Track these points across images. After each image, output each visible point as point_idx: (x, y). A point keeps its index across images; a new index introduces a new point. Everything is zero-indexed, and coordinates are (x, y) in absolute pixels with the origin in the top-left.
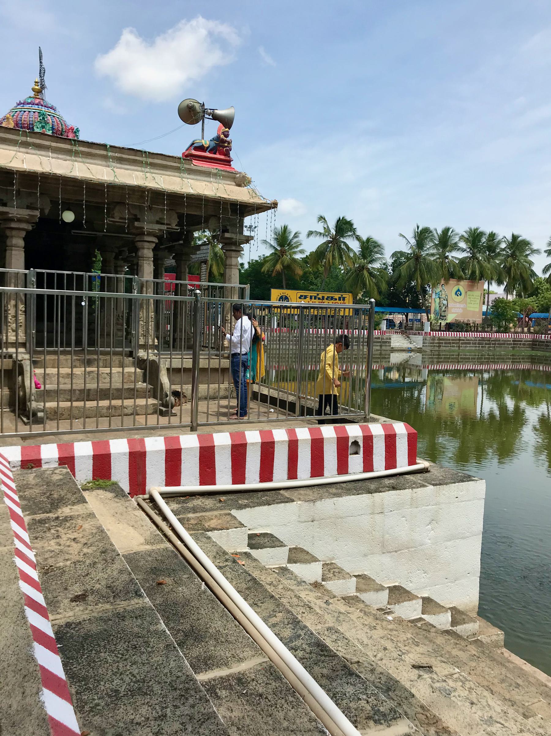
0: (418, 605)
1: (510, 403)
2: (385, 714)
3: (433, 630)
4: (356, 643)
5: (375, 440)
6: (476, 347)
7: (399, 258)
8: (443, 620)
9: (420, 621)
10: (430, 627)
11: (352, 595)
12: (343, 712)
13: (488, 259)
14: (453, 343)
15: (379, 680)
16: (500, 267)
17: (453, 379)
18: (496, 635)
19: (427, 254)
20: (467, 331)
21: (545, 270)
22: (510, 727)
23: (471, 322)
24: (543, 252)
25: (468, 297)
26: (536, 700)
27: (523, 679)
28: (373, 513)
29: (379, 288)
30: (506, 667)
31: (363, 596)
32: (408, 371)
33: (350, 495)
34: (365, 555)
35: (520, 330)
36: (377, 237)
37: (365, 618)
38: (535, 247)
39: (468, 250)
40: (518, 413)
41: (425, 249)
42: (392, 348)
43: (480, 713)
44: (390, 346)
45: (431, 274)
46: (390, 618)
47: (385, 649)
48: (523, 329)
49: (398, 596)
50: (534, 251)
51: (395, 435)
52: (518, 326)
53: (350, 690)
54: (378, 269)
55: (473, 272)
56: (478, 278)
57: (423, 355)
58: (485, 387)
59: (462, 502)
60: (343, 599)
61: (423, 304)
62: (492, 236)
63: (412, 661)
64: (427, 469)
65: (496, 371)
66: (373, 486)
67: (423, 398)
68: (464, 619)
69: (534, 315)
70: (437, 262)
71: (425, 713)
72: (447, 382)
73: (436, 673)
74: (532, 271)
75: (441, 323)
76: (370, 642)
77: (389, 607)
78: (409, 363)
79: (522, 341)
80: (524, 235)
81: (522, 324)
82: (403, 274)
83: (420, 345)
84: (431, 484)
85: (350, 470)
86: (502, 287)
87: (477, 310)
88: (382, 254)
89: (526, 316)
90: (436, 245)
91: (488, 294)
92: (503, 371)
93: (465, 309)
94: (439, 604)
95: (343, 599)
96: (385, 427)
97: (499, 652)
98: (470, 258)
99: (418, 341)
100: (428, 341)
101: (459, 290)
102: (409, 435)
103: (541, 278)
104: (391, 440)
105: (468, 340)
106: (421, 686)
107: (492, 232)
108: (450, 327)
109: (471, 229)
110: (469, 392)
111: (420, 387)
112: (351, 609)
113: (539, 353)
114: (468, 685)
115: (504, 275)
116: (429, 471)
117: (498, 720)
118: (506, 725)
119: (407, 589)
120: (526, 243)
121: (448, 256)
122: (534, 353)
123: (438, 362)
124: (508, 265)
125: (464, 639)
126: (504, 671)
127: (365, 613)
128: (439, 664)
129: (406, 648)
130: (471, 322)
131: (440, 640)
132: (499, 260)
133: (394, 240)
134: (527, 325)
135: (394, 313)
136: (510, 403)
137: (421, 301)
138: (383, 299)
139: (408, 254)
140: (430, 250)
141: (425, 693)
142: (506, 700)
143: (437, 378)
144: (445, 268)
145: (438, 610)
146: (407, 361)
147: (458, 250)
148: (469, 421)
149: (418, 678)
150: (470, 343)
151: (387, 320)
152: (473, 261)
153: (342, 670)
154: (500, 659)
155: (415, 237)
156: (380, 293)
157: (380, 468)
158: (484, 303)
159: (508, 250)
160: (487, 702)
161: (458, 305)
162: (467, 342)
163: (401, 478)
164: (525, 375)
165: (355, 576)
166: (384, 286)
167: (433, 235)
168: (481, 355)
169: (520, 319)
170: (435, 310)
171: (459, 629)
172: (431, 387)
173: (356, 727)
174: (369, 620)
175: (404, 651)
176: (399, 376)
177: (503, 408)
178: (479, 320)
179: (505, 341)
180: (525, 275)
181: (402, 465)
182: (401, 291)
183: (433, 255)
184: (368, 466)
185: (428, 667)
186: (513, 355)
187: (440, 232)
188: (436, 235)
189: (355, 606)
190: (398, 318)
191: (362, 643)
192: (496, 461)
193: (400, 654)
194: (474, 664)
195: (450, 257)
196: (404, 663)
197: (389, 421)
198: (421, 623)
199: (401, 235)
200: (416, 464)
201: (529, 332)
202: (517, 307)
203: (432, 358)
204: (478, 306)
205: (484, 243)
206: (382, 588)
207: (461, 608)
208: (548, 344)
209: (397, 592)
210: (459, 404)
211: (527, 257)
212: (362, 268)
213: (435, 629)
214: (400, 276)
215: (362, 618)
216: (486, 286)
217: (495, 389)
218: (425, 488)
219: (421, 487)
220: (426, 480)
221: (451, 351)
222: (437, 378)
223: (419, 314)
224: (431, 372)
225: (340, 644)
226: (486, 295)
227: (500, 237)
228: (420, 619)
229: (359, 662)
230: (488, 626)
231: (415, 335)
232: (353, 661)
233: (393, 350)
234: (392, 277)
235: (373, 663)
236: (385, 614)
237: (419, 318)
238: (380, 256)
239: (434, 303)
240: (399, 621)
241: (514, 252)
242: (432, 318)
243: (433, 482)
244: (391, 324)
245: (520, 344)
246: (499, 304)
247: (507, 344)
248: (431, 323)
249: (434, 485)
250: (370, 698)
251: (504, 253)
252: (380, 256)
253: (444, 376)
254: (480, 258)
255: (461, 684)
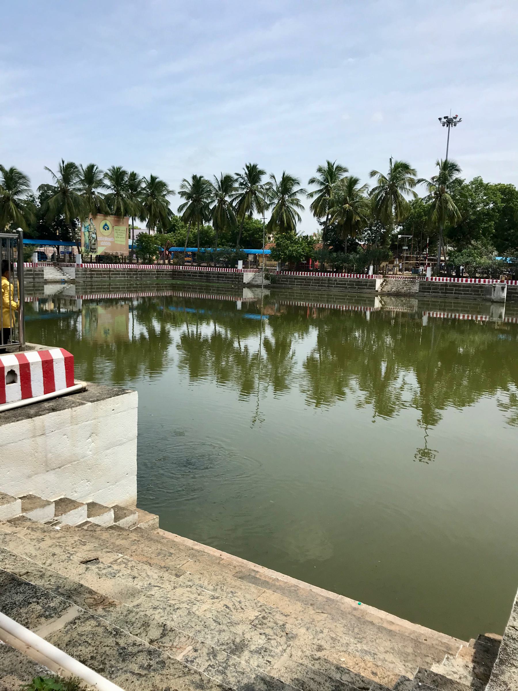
0: (83, 511)
1: (157, 326)
2: (55, 608)
3: (99, 528)
4: (24, 556)
5: (32, 368)
6: (125, 277)
7: (46, 191)
8: (106, 519)
9: (86, 524)
10: (95, 527)
11: (18, 516)
12: (14, 619)
13: (131, 197)
14: (104, 274)
15: (49, 583)
16: (142, 205)
17: (106, 307)
18: (153, 519)
19: (74, 189)
20: (116, 263)
21: (180, 209)
22: (166, 587)
23: (119, 254)
24: (177, 193)
25: (115, 231)
26: (185, 562)
27: (175, 548)
28: (34, 436)
29: (27, 220)
30: (161, 543)
31: (29, 515)
32: (62, 302)
33: (9, 423)
34: (29, 477)
35: (161, 262)
36: (21, 168)
37: (32, 533)
38: (170, 188)
39: (113, 187)
40: (164, 334)
41: (72, 183)
42: (46, 280)
43: (141, 584)
44: (43, 278)
45: (79, 209)
46: (58, 528)
47: (54, 555)
48: (164, 262)
49: (64, 507)
50: (169, 192)
51: (52, 361)
52: (160, 258)
53: (20, 598)
54: (25, 201)
55: (119, 209)
56: (123, 213)
57: (76, 286)
58: (135, 313)
59: (118, 413)
60: (8, 521)
61: (74, 237)
62: (133, 176)
63: (80, 559)
64: (85, 388)
65: (143, 298)
66: (32, 411)
67: (79, 327)
68: (125, 514)
69: (172, 249)
70: (84, 197)
71: (93, 596)
72: (101, 310)
73: (102, 563)
74: (169, 209)
75: (91, 256)
76: (38, 553)
77: (56, 518)
78: (64, 294)
79: (164, 272)
80: (161, 177)
81: (163, 256)
82: (51, 207)
83: (73, 277)
84: (89, 401)
85: (8, 399)
86: (145, 223)
87: (124, 243)
88: (27, 186)
89: (166, 250)
90: (81, 180)
91: (133, 229)
92: (150, 298)
93: (113, 243)
94: (102, 506)
95: (8, 521)
96: (41, 353)
97: (156, 533)
98: (115, 195)
99: (71, 273)
100: (80, 273)
101: (106, 225)
102: (66, 359)
103: (177, 216)
104: (48, 366)
105: (118, 271)
106: (89, 576)
107: (133, 172)
108: (100, 259)
109: (114, 168)
110: (120, 319)
111: (75, 317)
112: (17, 529)
113: (179, 282)
114: (130, 565)
115: (145, 212)
116: (87, 390)
117: (156, 585)
118: (162, 586)
119: (73, 499)
120: (162, 185)
121: (94, 192)
122: (174, 282)
123: (91, 293)
124: (148, 203)
125: (126, 530)
126: (159, 546)
127: (33, 529)
128: (105, 555)
129: (74, 550)
130: (119, 254)
131: (105, 535)
132: (140, 198)
133: (40, 174)
134: (168, 258)
135: (45, 245)
136: (157, 326)
137: (71, 234)
138: (33, 231)
139: (55, 187)
140: (76, 185)
141: (92, 581)
142: (161, 567)
143: (91, 307)
144: (92, 203)
145: (102, 511)
146: (62, 292)
147: (103, 187)
148: (123, 344)
149: (86, 571)
150: (119, 274)
151: (38, 252)
152: (118, 198)
153: (10, 583)
154: (156, 538)
155: (61, 171)
156: (29, 225)
157: (38, 393)
158: (129, 238)
159: (148, 190)
160: (146, 573)
161: (106, 239)
162: (117, 273)
163: (60, 400)
164: (168, 301)
165: (20, 498)
166: (32, 219)
167: (78, 171)
168: (130, 285)
169: (161, 253)
170: (85, 243)
171: (121, 523)
172: (86, 316)
173: (28, 628)
174: (38, 534)
175: (72, 553)
176: (55, 307)
177: (151, 331)
178: (126, 252)
179: (150, 271)
180: (163, 213)
181: (61, 387)
182: (50, 225)
183: (80, 190)
184: (26, 392)
185: (95, 559)
186: (157, 284)
187: (85, 167)
188: (81, 171)
189: (21, 525)
190: (50, 251)
191: (30, 556)
192: (147, 377)
193: (69, 556)
194: (134, 547)
195: (96, 193)
196: (73, 562)
197: (45, 348)
198: (87, 526)
199: (47, 168)
200: (74, 385)
201: (169, 263)
202: (158, 241)
203: (86, 288)
204: (124, 240)
205: (126, 182)
206: (48, 503)
207: (122, 505)
208: (185, 274)
209: (63, 504)
210: (113, 330)
211: (164, 197)
212: (7, 199)
213: (100, 528)
214: (48, 209)
215: (30, 534)
216: (130, 222)
217: (144, 313)
218: (84, 406)
219: (80, 405)
220: (84, 399)
221: (101, 282)
222: (91, 307)
223: (70, 247)
224: (85, 302)
225: (7, 562)
226: (131, 230)
227: (140, 177)
228: (87, 522)
229: (28, 572)
230: (146, 514)
231: (67, 266)
232: (21, 573)
233: (47, 282)
234: (40, 209)
235: (42, 570)
236: (52, 526)
237: (70, 250)
238: (26, 188)
239: (84, 237)
240: (67, 528)
241: (153, 192)
242: (83, 251)
243: (91, 400)
244: (42, 256)
245: (163, 274)
246: (142, 237)
247: (152, 274)
248: (82, 255)
249: (91, 402)
250: (40, 598)
251: (145, 192)
252: (26, 188)
253: (97, 304)
254: (124, 196)
255: (124, 565)
